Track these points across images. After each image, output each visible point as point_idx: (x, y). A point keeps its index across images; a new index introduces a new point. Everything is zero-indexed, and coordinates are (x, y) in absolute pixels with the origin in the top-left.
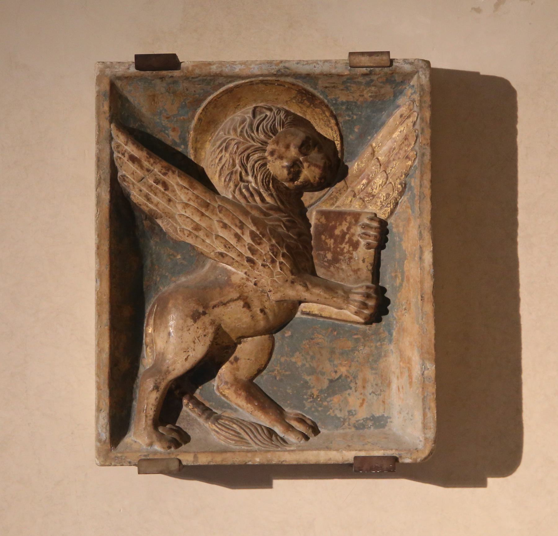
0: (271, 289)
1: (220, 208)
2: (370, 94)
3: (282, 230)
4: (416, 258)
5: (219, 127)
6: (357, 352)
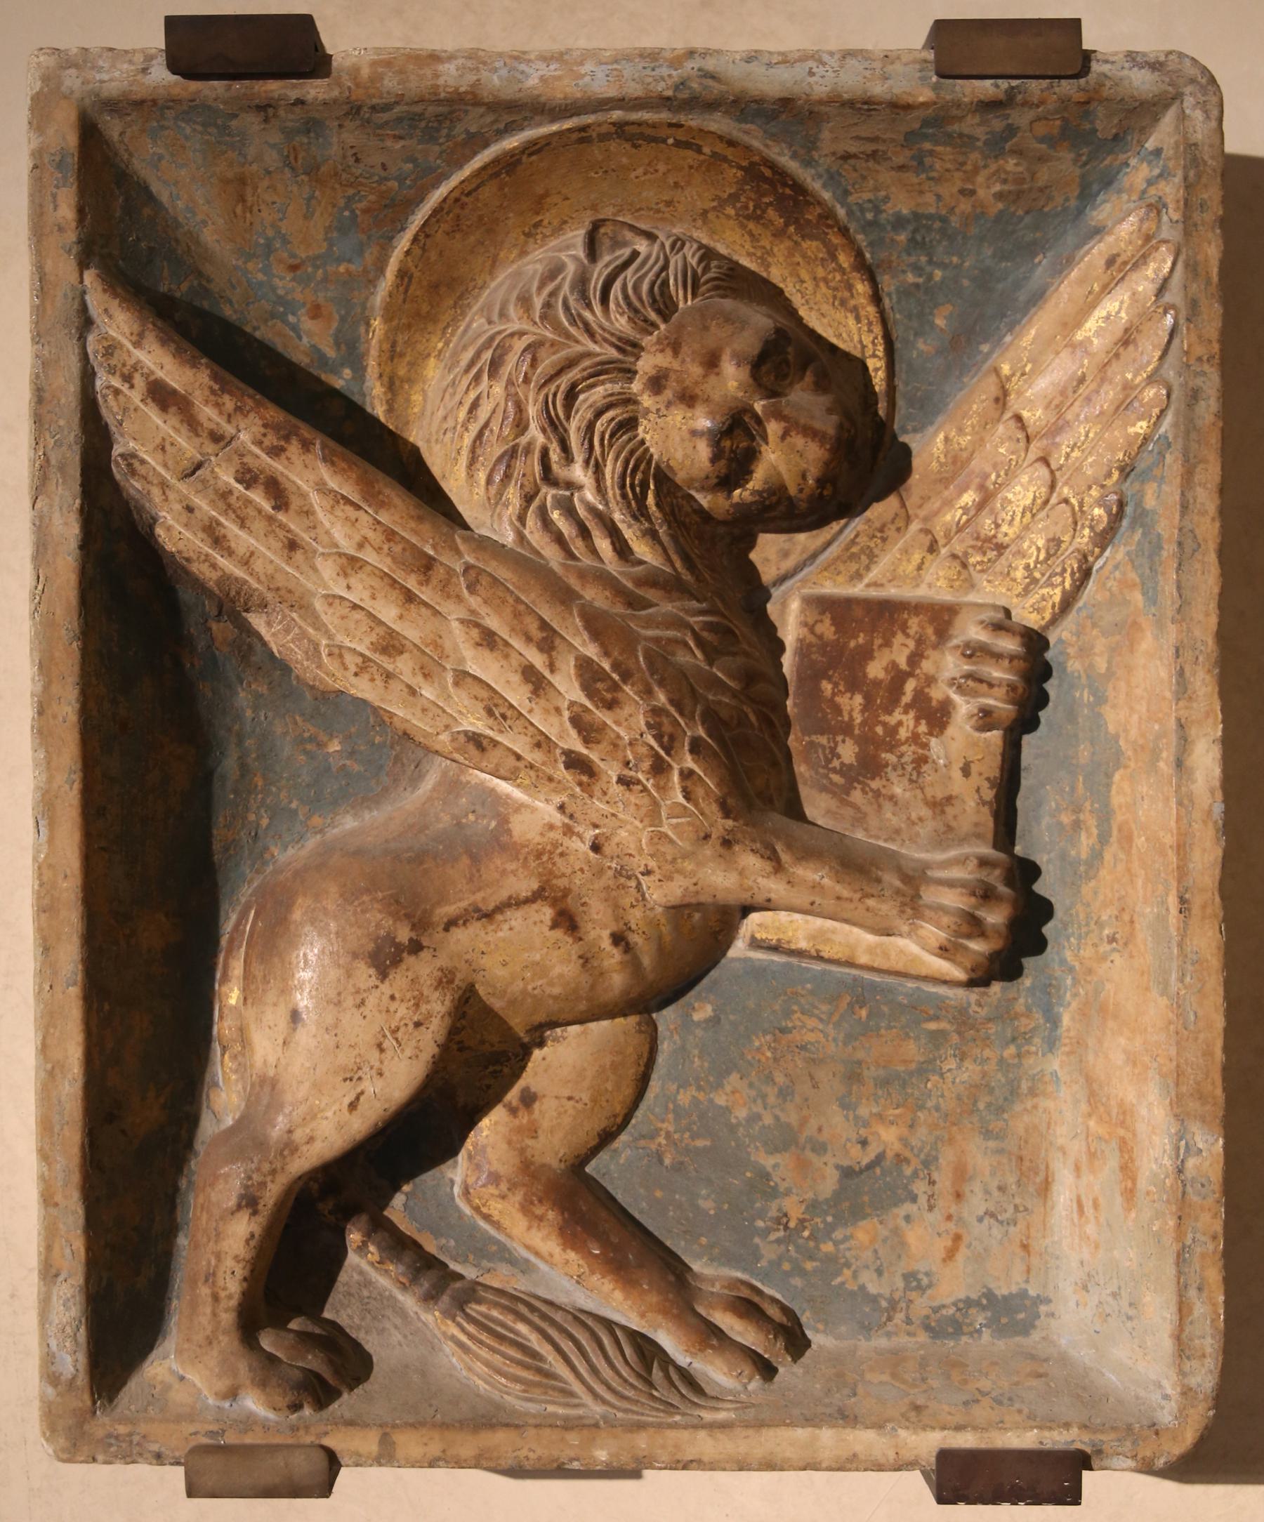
0: (652, 864)
1: (473, 573)
2: (997, 187)
3: (691, 658)
4: (1161, 764)
5: (469, 306)
6: (935, 1078)
